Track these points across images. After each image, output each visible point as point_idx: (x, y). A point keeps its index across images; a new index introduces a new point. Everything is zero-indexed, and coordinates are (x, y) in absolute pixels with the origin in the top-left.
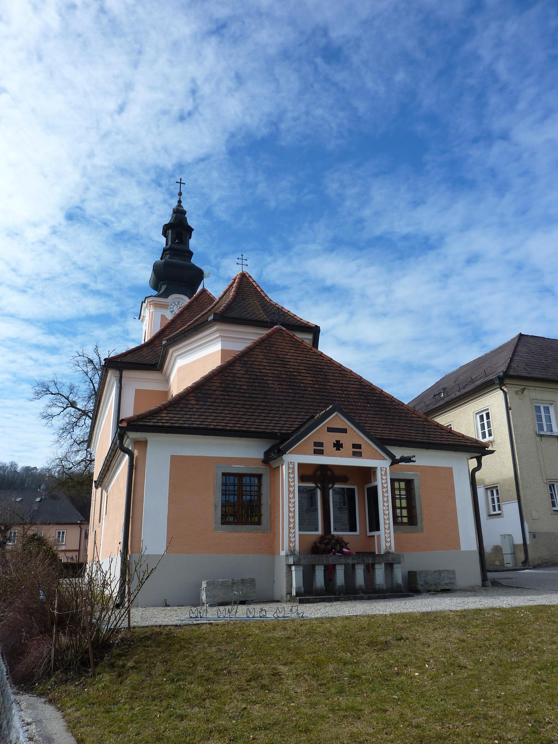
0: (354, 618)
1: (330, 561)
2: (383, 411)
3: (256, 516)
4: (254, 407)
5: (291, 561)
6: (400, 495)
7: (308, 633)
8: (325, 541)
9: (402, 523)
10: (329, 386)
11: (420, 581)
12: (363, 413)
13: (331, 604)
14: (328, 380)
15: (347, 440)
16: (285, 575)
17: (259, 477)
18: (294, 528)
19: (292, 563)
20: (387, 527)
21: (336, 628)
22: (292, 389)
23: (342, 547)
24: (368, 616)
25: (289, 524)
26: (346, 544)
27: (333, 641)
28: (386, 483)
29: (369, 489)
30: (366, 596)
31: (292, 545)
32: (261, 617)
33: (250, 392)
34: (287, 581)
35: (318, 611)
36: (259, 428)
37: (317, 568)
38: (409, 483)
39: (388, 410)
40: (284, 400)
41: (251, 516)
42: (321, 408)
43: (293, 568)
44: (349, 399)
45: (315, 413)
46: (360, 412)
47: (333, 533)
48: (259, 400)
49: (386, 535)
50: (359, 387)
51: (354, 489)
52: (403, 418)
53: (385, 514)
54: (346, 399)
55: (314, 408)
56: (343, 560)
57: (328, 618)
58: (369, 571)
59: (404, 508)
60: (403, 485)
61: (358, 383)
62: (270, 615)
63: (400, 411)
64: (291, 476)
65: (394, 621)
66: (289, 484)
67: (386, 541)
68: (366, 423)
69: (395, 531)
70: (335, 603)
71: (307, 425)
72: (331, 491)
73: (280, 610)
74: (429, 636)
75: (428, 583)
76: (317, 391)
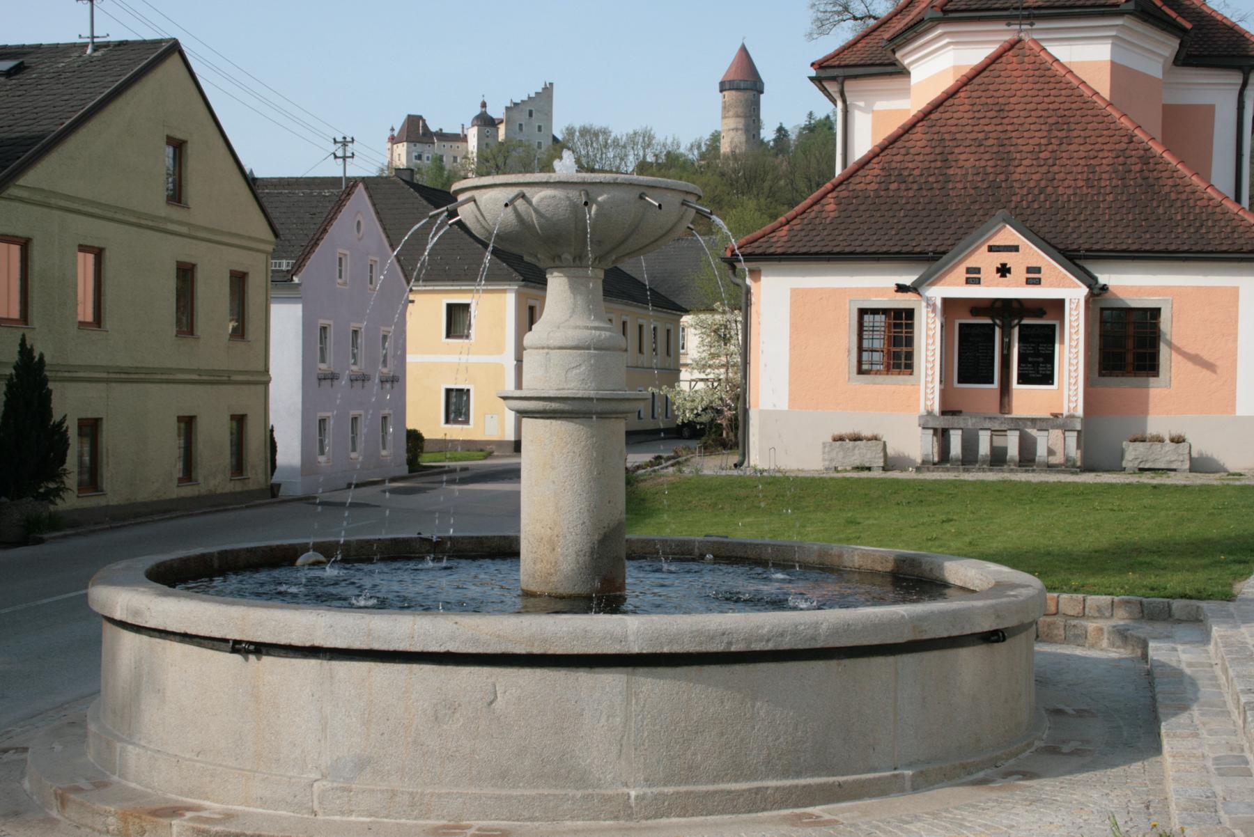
15: (1017, 262)
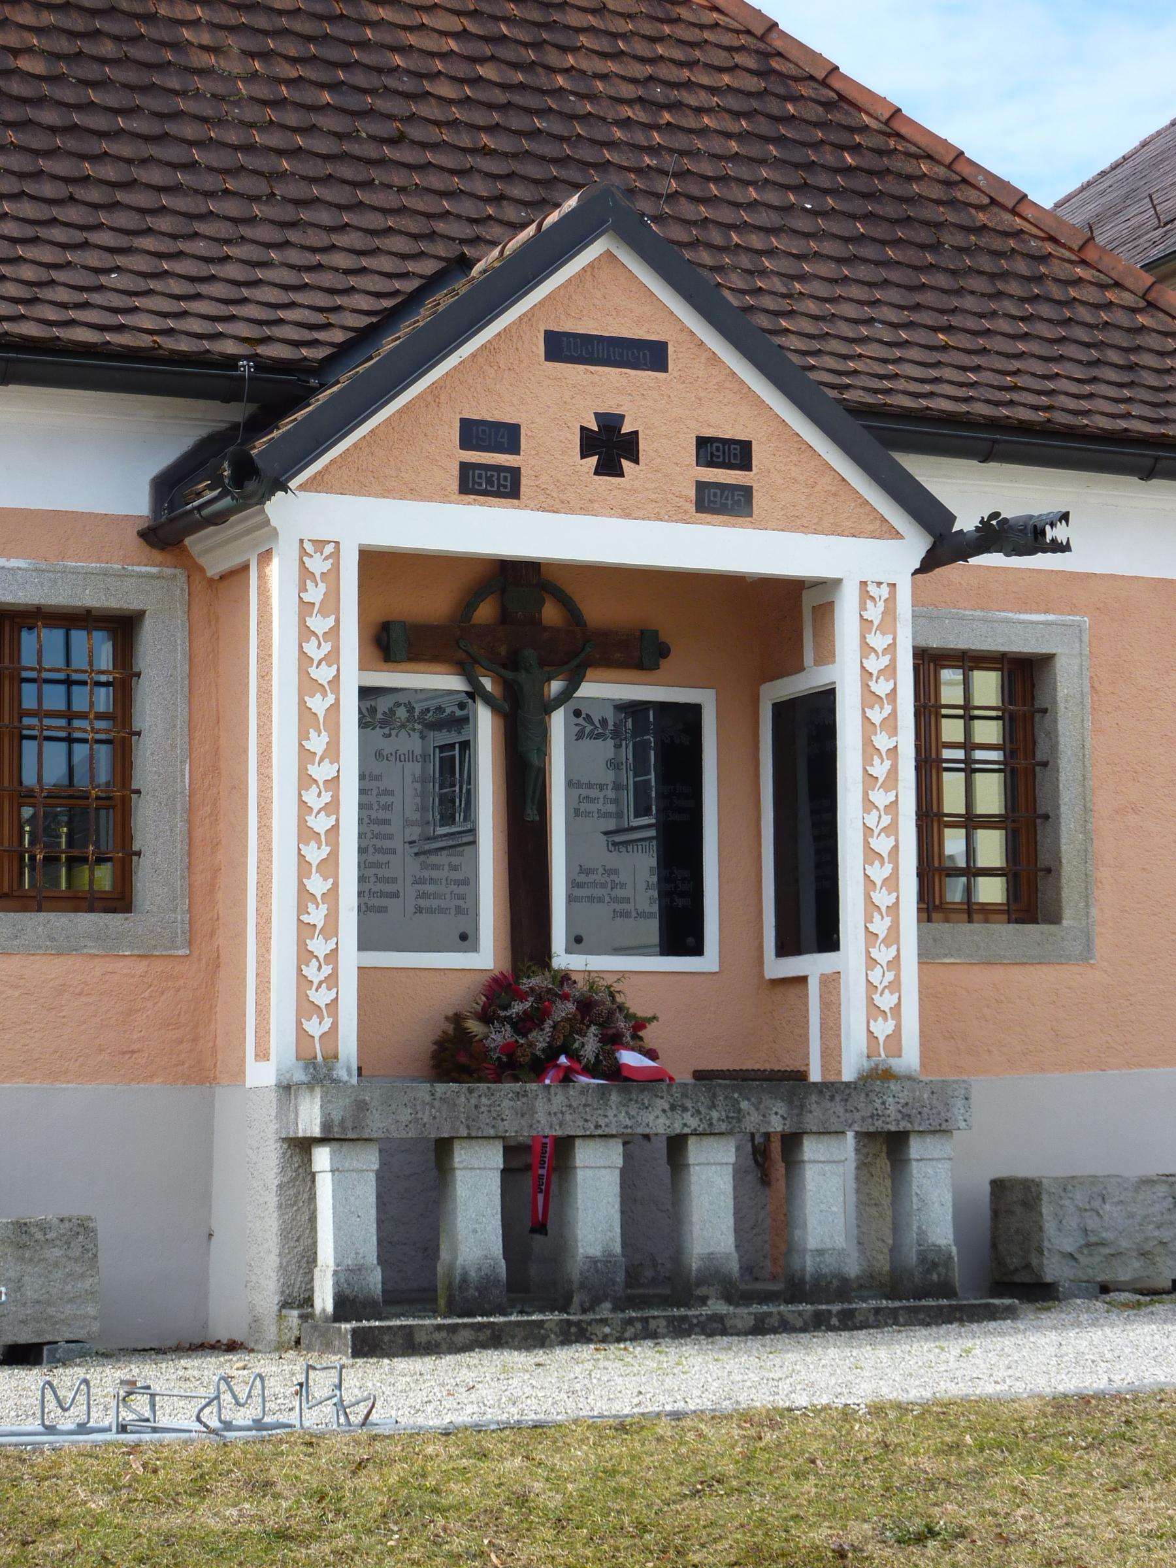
0: (664, 1428)
1: (541, 1116)
2: (896, 243)
3: (100, 860)
4: (94, 195)
5: (309, 1117)
6: (968, 745)
7: (399, 1509)
8: (518, 1008)
9: (972, 911)
10: (567, 71)
11: (1058, 1238)
12: (771, 253)
13: (540, 1356)
14: (560, 38)
16: (272, 1199)
17: (123, 628)
18: (331, 928)
19: (316, 1132)
20: (880, 926)
21: (556, 1480)
22: (334, 86)
23: (612, 1040)
24: (746, 1417)
25: (302, 909)
26: (640, 1025)
27: (539, 1550)
28: (891, 671)
29: (784, 711)
30: (744, 1314)
31: (315, 1028)
32: (123, 1429)
33: (68, 95)
34: (285, 1233)
35: (463, 1396)
36: (121, 328)
37: (461, 1156)
38: (1025, 677)
39: (923, 235)
40: (281, 153)
41: (74, 862)
42: (511, 213)
43: (322, 1158)
44: (687, 163)
45: (476, 241)
46: (756, 241)
47: (562, 958)
48: (125, 149)
49: (876, 976)
50: (753, 84)
51: (695, 710)
52: (1014, 288)
53: (871, 855)
54: (670, 162)
55: (468, 208)
56: (617, 1114)
57: (517, 1427)
58: (765, 1180)
59: (988, 822)
60: (987, 687)
61: (750, 62)
62: (177, 1416)
63: (998, 244)
64: (319, 624)
65: (892, 1439)
66: (303, 673)
67: (874, 1011)
68: (791, 314)
69: (925, 956)
70: (562, 1354)
71: (423, 315)
72: (558, 722)
73: (242, 1392)
74: (1083, 1519)
75: (1103, 1243)
76: (491, 106)
